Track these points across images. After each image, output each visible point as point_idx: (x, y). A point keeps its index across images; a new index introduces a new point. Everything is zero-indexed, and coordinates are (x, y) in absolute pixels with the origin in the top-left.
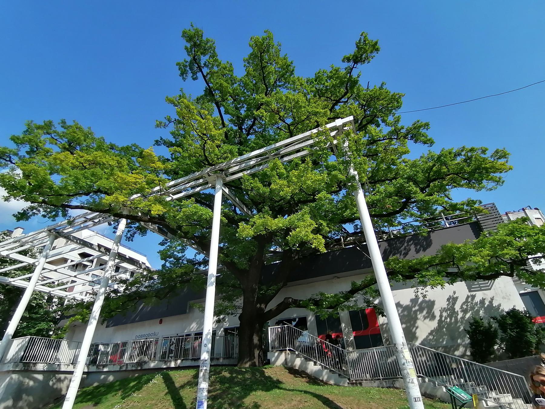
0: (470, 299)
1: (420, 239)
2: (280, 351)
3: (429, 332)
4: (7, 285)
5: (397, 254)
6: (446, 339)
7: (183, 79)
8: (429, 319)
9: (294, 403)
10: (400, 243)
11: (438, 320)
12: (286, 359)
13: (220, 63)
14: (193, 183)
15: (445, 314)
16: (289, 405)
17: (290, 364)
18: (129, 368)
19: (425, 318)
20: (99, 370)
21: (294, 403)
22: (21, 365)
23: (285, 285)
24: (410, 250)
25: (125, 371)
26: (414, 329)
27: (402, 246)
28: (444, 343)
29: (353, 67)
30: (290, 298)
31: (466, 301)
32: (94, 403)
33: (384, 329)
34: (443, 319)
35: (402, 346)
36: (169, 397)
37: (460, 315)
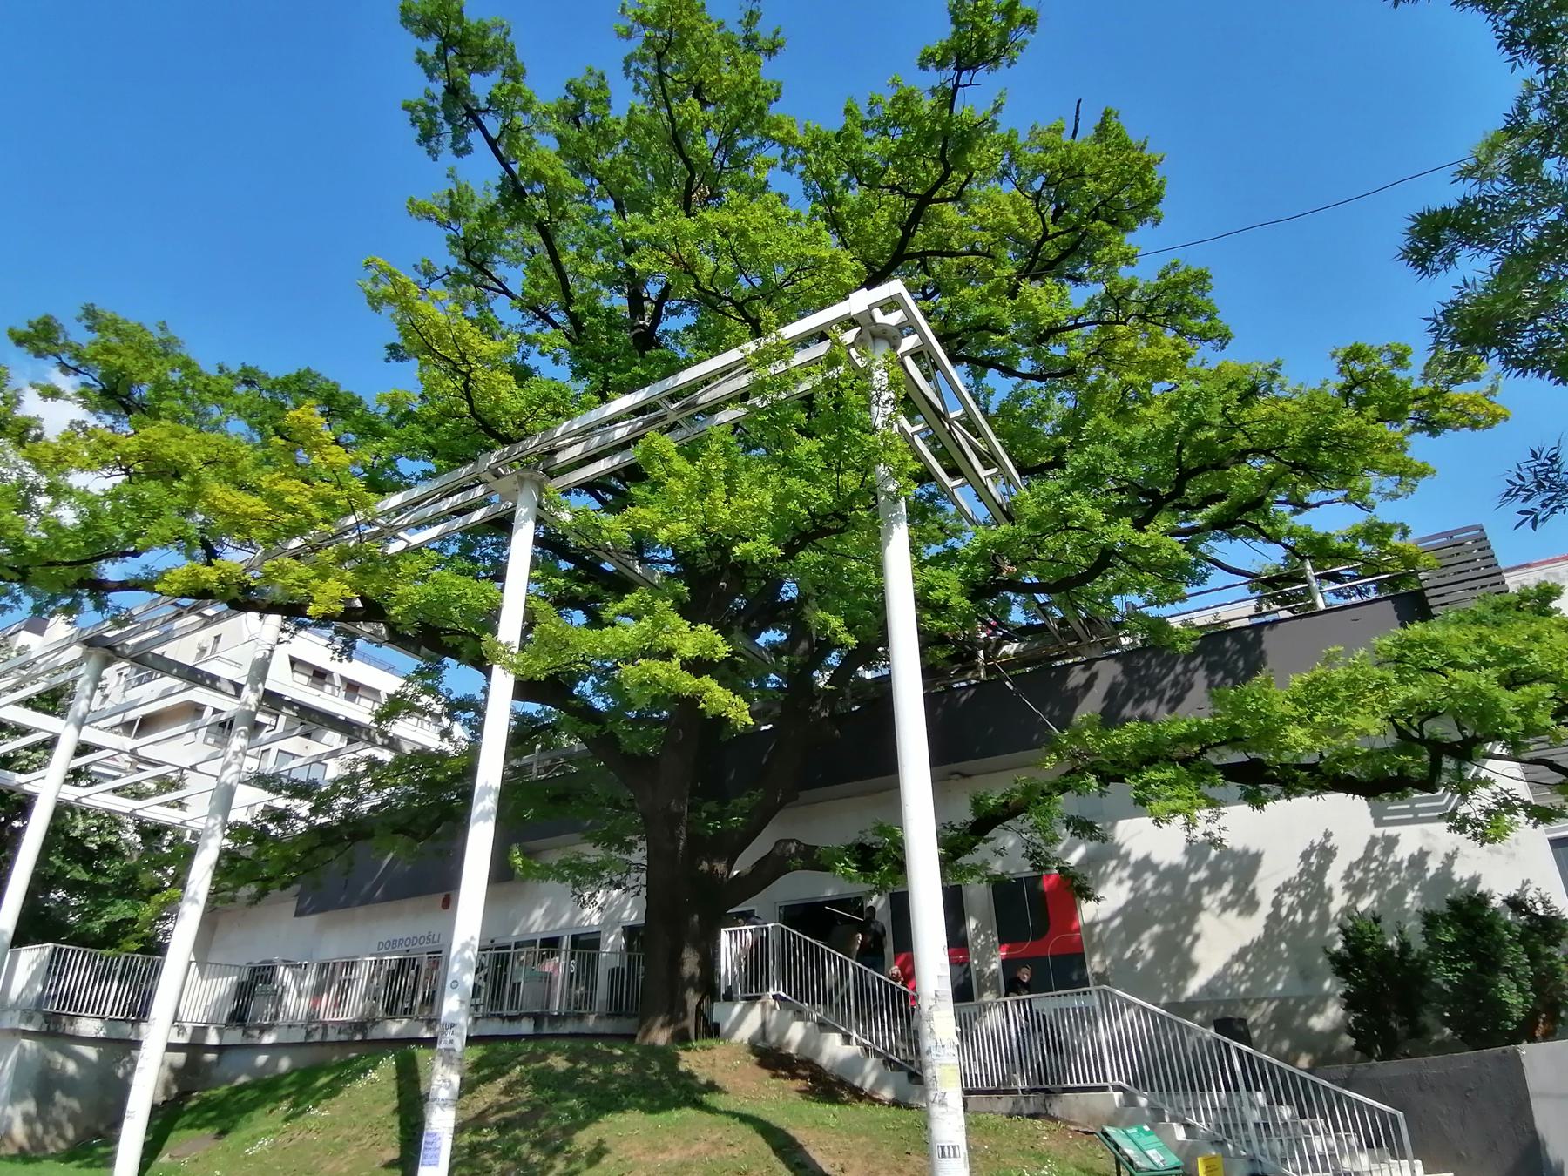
0: (1377, 852)
1: (1227, 650)
2: (747, 999)
3: (1235, 950)
4: (12, 792)
5: (1150, 698)
6: (1284, 977)
7: (429, 153)
8: (1236, 911)
9: (701, 1147)
10: (1161, 665)
11: (1269, 917)
12: (764, 1024)
13: (530, 101)
14: (456, 499)
15: (1288, 900)
16: (685, 1153)
17: (773, 1038)
18: (332, 1036)
19: (1225, 906)
20: (250, 1041)
21: (701, 1147)
22: (39, 1018)
23: (790, 798)
24: (1191, 686)
25: (322, 1043)
26: (1189, 940)
27: (1167, 675)
28: (1279, 986)
29: (956, 86)
30: (792, 841)
31: (1367, 857)
32: (217, 1130)
33: (1095, 939)
34: (1284, 911)
35: (933, 1003)
36: (395, 1120)
37: (1339, 901)
